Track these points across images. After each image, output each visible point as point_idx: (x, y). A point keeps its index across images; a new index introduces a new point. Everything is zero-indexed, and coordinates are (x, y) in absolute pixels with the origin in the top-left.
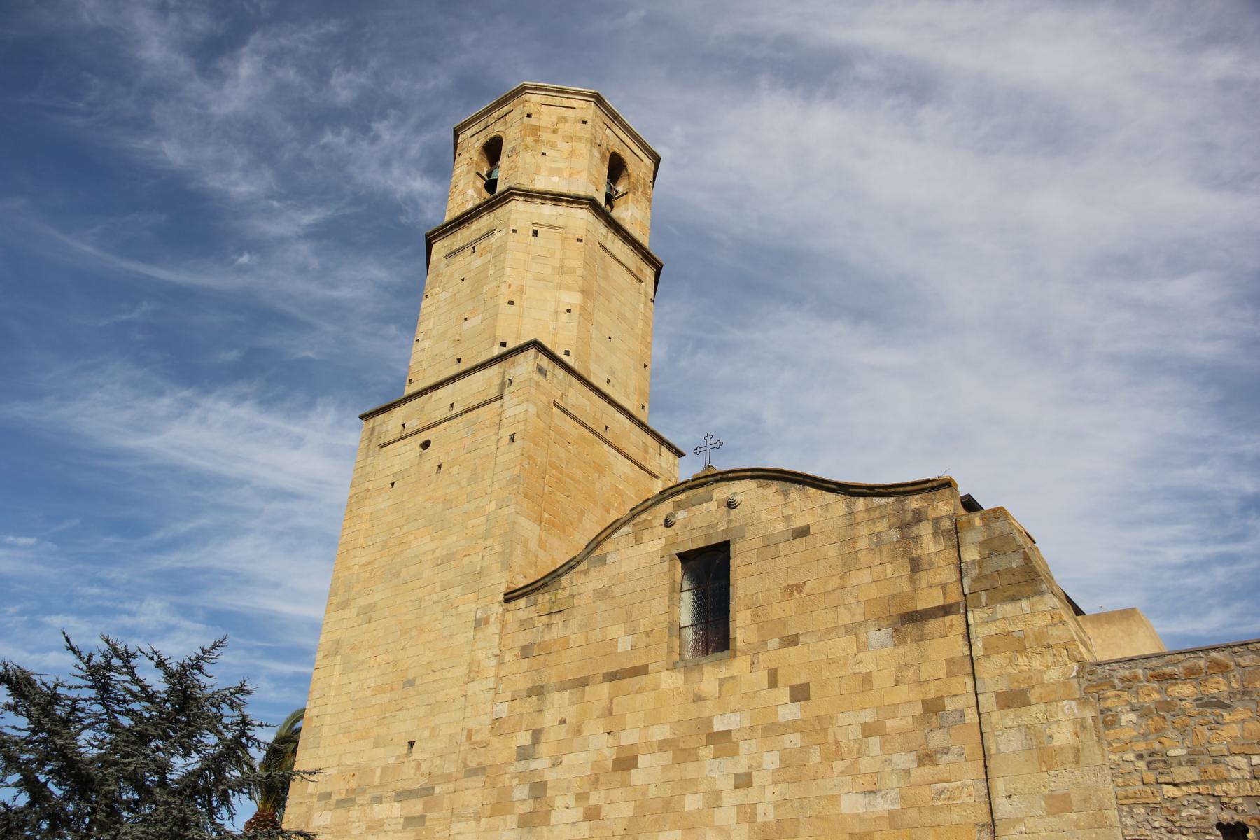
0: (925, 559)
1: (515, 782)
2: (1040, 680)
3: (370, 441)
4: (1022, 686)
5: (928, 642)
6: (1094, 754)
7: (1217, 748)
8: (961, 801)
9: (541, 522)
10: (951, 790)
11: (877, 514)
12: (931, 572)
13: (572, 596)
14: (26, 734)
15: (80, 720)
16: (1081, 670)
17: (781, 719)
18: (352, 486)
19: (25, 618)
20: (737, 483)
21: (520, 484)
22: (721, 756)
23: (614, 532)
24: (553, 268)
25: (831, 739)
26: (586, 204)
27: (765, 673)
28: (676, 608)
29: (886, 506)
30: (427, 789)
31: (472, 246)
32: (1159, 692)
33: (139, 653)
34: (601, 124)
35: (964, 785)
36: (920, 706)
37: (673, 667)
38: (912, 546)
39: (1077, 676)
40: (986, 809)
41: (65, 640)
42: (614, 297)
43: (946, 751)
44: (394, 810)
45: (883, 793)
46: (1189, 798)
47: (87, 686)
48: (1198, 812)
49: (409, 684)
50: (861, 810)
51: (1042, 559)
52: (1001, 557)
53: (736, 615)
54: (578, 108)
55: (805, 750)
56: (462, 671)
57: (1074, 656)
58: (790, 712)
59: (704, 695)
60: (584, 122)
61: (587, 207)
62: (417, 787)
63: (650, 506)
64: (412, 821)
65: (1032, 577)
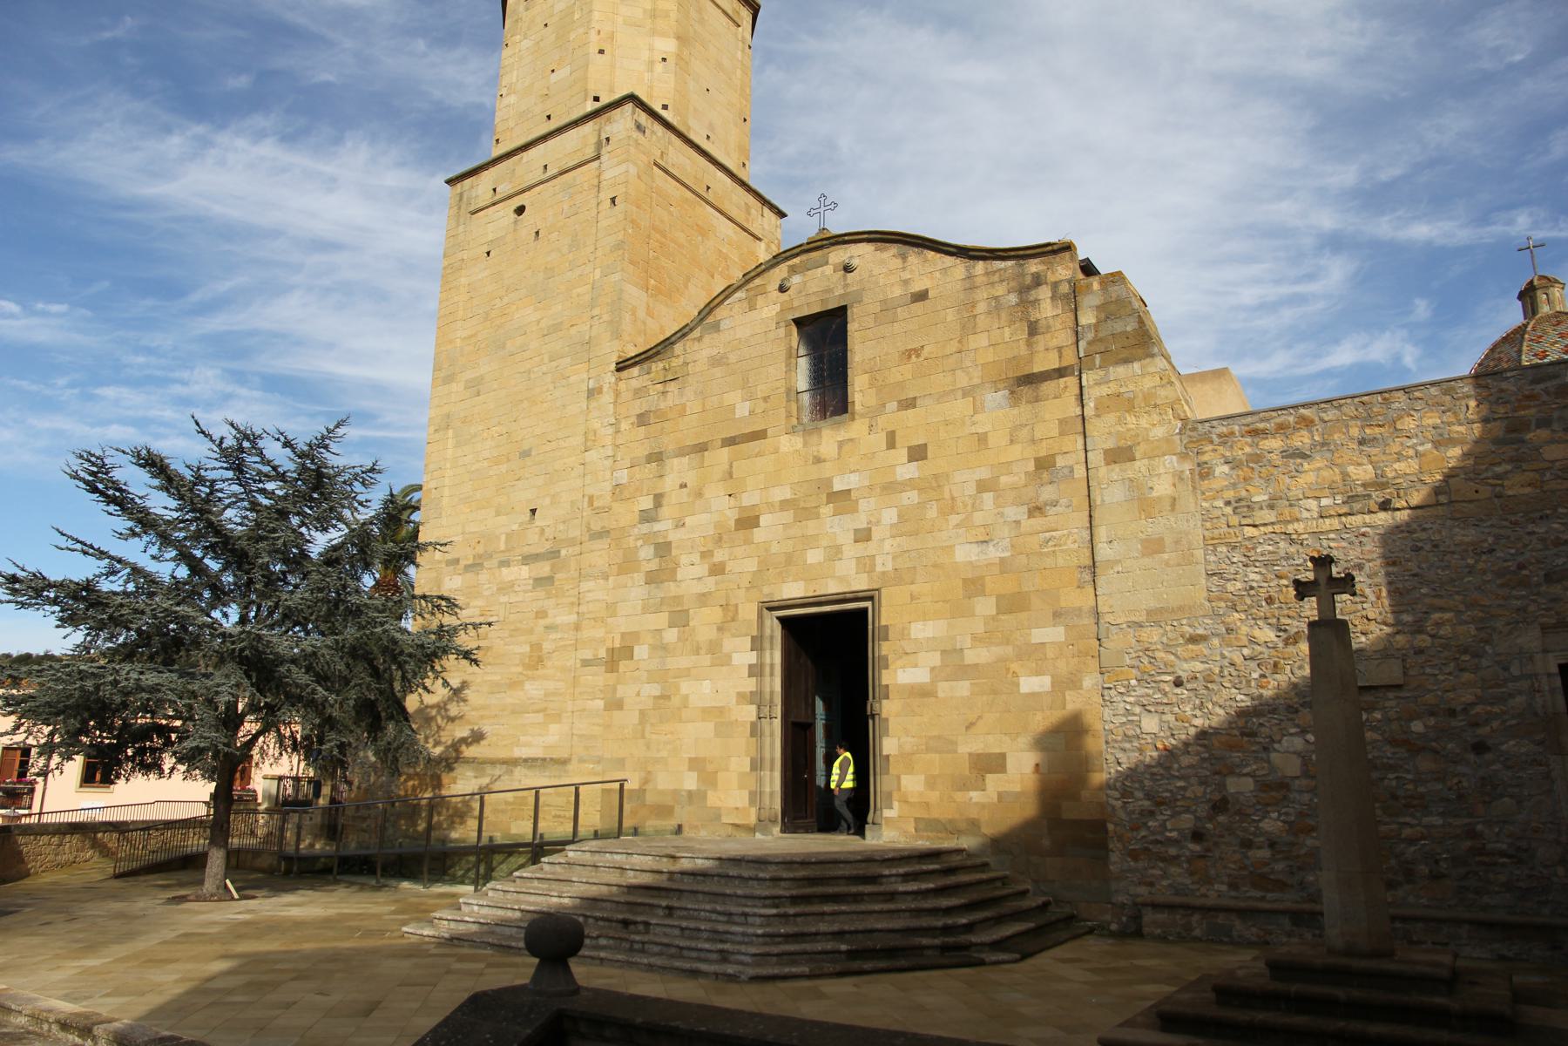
0: (1043, 322)
1: (640, 543)
3: (459, 208)
6: (1189, 502)
7: (1295, 493)
9: (648, 289)
11: (996, 278)
12: (1048, 336)
14: (175, 515)
15: (220, 499)
17: (899, 479)
18: (445, 256)
19: (76, 391)
20: (853, 246)
23: (727, 297)
24: (645, 11)
25: (947, 495)
27: (883, 435)
28: (793, 373)
29: (1005, 270)
32: (1251, 446)
33: (265, 435)
37: (792, 431)
39: (1180, 433)
40: (1088, 553)
41: (194, 424)
43: (1055, 504)
46: (1266, 537)
47: (222, 468)
48: (1270, 548)
49: (526, 454)
50: (974, 558)
51: (1153, 322)
55: (921, 505)
56: (577, 440)
57: (1179, 415)
58: (908, 471)
62: (543, 550)
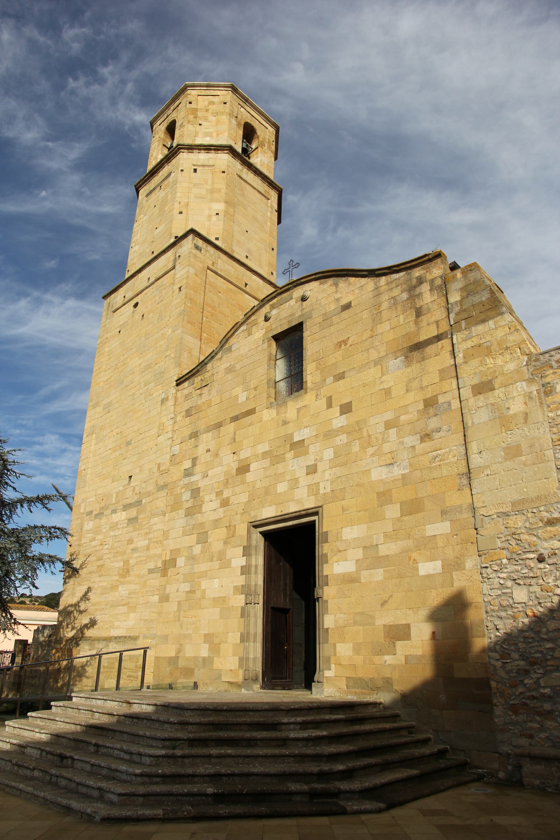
0: (425, 307)
1: (183, 490)
2: (501, 372)
3: (108, 310)
4: (489, 378)
5: (427, 361)
6: (538, 415)
8: (449, 461)
10: (442, 455)
11: (394, 285)
13: (213, 375)
16: (529, 359)
17: (334, 427)
20: (307, 285)
21: (184, 315)
22: (298, 457)
23: (236, 331)
24: (207, 190)
25: (365, 434)
26: (226, 150)
29: (399, 279)
30: (138, 502)
31: (159, 185)
34: (237, 105)
35: (451, 450)
36: (422, 403)
38: (416, 301)
39: (527, 365)
42: (249, 208)
43: (439, 430)
44: (122, 516)
45: (398, 463)
49: (129, 443)
50: (384, 477)
52: (476, 295)
53: (307, 367)
54: (221, 95)
56: (154, 431)
57: (525, 352)
58: (340, 421)
59: (288, 420)
60: (225, 103)
61: (227, 152)
62: (133, 501)
63: (256, 311)
64: (132, 521)
65: (496, 304)
